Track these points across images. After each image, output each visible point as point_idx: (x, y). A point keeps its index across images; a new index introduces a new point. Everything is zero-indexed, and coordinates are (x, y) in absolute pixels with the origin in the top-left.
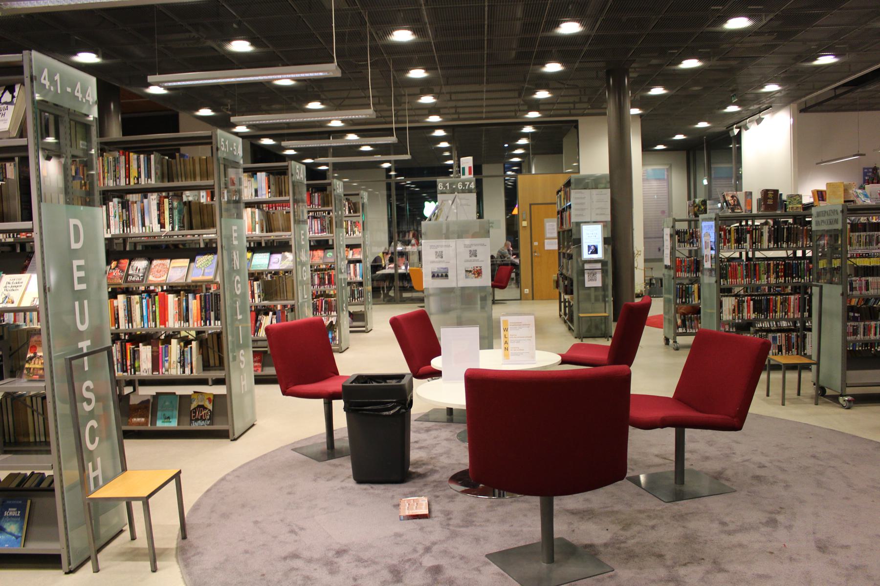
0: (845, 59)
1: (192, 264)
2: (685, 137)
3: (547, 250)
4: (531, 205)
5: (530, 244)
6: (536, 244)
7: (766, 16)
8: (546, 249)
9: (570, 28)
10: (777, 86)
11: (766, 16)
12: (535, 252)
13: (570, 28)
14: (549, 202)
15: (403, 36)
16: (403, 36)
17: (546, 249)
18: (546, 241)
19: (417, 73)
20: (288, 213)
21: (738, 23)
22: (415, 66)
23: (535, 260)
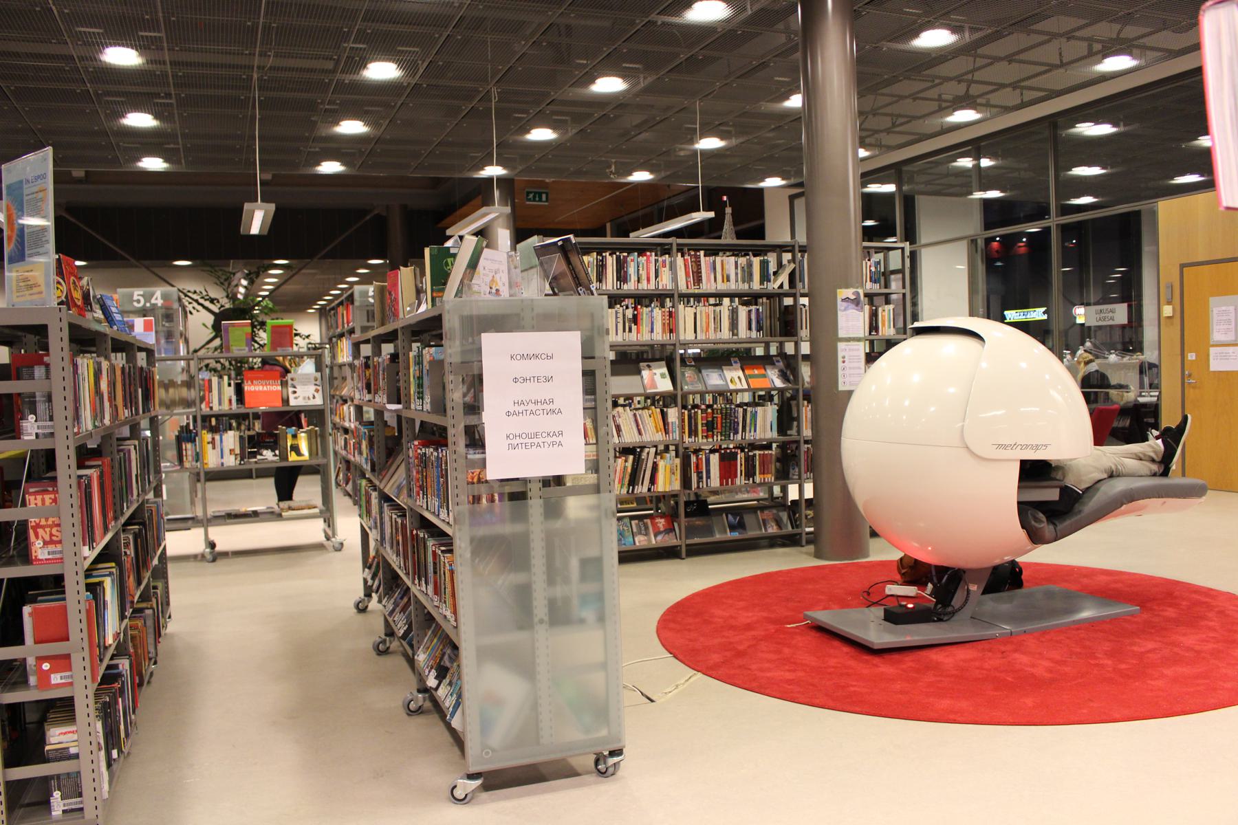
0: (734, 142)
1: (1209, 487)
2: (1103, 171)
3: (1214, 372)
4: (1183, 266)
5: (1179, 358)
6: (1191, 356)
7: (645, 78)
8: (1212, 369)
9: (382, 71)
10: (648, 173)
11: (645, 78)
12: (1190, 376)
13: (382, 71)
14: (1219, 257)
15: (122, 57)
16: (122, 57)
17: (1212, 369)
18: (1212, 351)
19: (139, 120)
20: (348, 323)
21: (609, 85)
22: (138, 107)
23: (1190, 393)
